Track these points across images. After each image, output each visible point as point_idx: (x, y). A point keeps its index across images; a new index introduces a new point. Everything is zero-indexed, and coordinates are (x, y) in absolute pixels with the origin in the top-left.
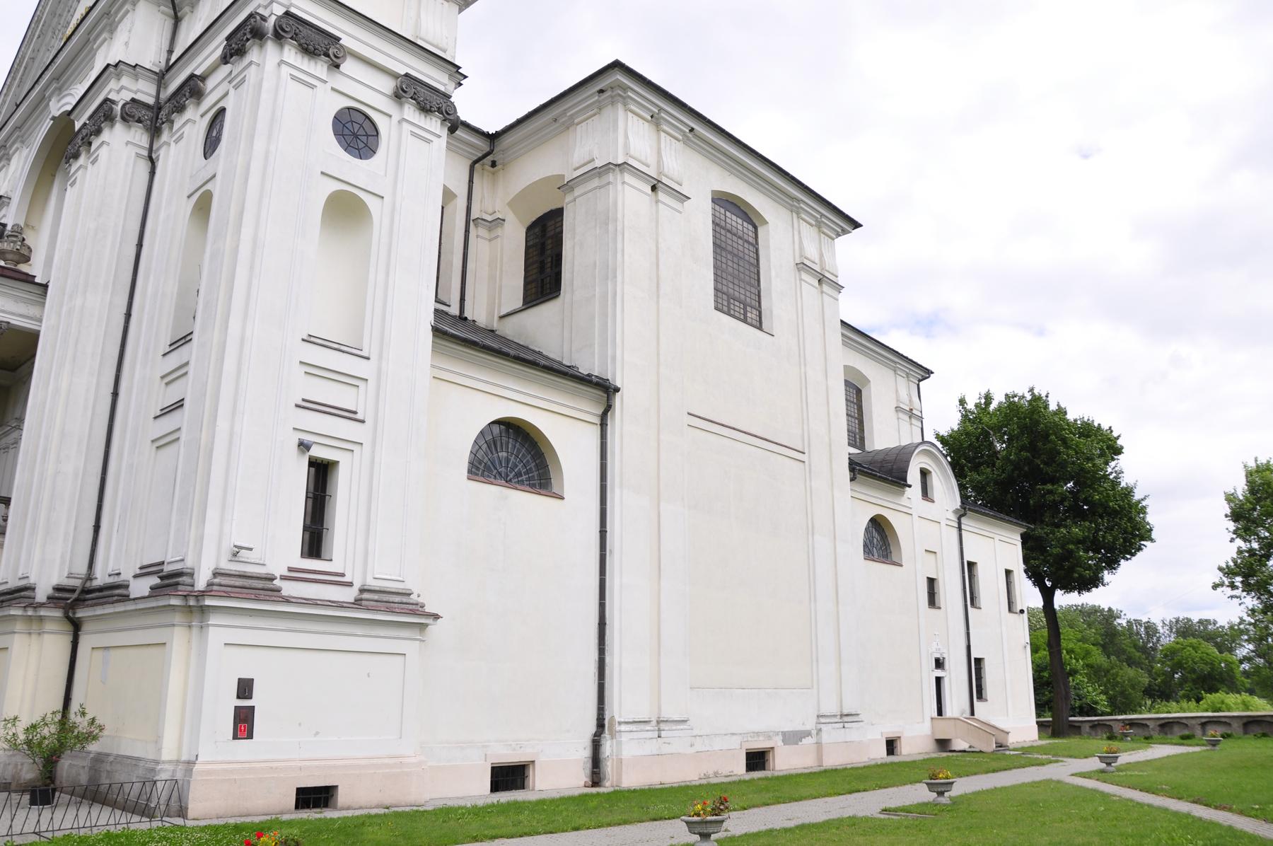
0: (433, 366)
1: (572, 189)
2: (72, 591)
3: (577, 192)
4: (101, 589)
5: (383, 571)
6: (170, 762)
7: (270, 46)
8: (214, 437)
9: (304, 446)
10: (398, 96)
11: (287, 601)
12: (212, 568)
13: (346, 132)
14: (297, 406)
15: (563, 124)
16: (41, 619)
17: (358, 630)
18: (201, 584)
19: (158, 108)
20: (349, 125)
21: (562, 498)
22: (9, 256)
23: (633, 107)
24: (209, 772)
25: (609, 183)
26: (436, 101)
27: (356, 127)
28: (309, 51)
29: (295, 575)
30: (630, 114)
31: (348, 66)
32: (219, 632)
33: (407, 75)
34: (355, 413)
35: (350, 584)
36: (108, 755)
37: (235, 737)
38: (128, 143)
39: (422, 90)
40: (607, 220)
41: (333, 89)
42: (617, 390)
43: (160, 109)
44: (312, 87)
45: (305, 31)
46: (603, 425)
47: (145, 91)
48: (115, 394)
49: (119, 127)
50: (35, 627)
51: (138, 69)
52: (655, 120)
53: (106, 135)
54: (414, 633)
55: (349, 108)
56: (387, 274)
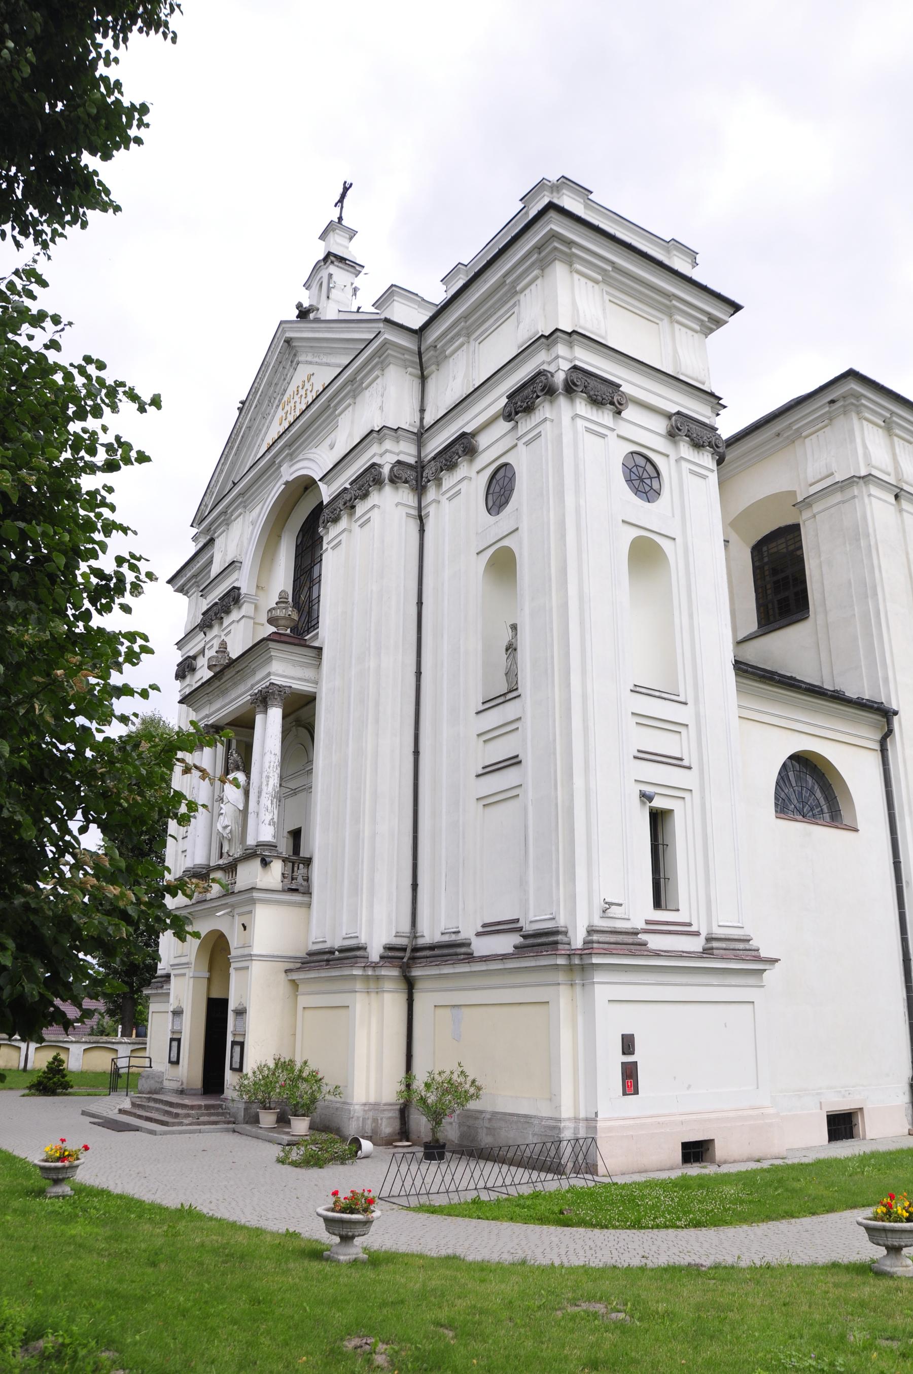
0: (739, 706)
1: (810, 505)
2: (404, 949)
3: (816, 508)
4: (432, 948)
5: (725, 920)
6: (569, 1119)
7: (562, 401)
8: (572, 795)
9: (646, 797)
10: (672, 435)
11: (657, 954)
12: (586, 926)
13: (634, 477)
14: (635, 757)
15: (788, 437)
16: (378, 978)
17: (714, 980)
18: (578, 939)
19: (419, 467)
20: (634, 470)
21: (857, 830)
22: (282, 622)
23: (867, 415)
24: (610, 1129)
25: (854, 497)
26: (706, 435)
27: (641, 470)
28: (596, 402)
29: (653, 927)
30: (865, 423)
31: (630, 412)
32: (605, 989)
33: (678, 413)
34: (681, 759)
35: (697, 934)
36: (481, 1112)
37: (624, 1094)
38: (397, 504)
39: (693, 426)
40: (858, 537)
41: (619, 436)
42: (896, 713)
43: (423, 467)
44: (603, 436)
45: (592, 383)
46: (883, 751)
47: (406, 452)
48: (416, 753)
49: (388, 489)
50: (372, 985)
51: (400, 432)
52: (888, 427)
53: (375, 498)
54: (751, 980)
55: (632, 453)
56: (691, 616)
